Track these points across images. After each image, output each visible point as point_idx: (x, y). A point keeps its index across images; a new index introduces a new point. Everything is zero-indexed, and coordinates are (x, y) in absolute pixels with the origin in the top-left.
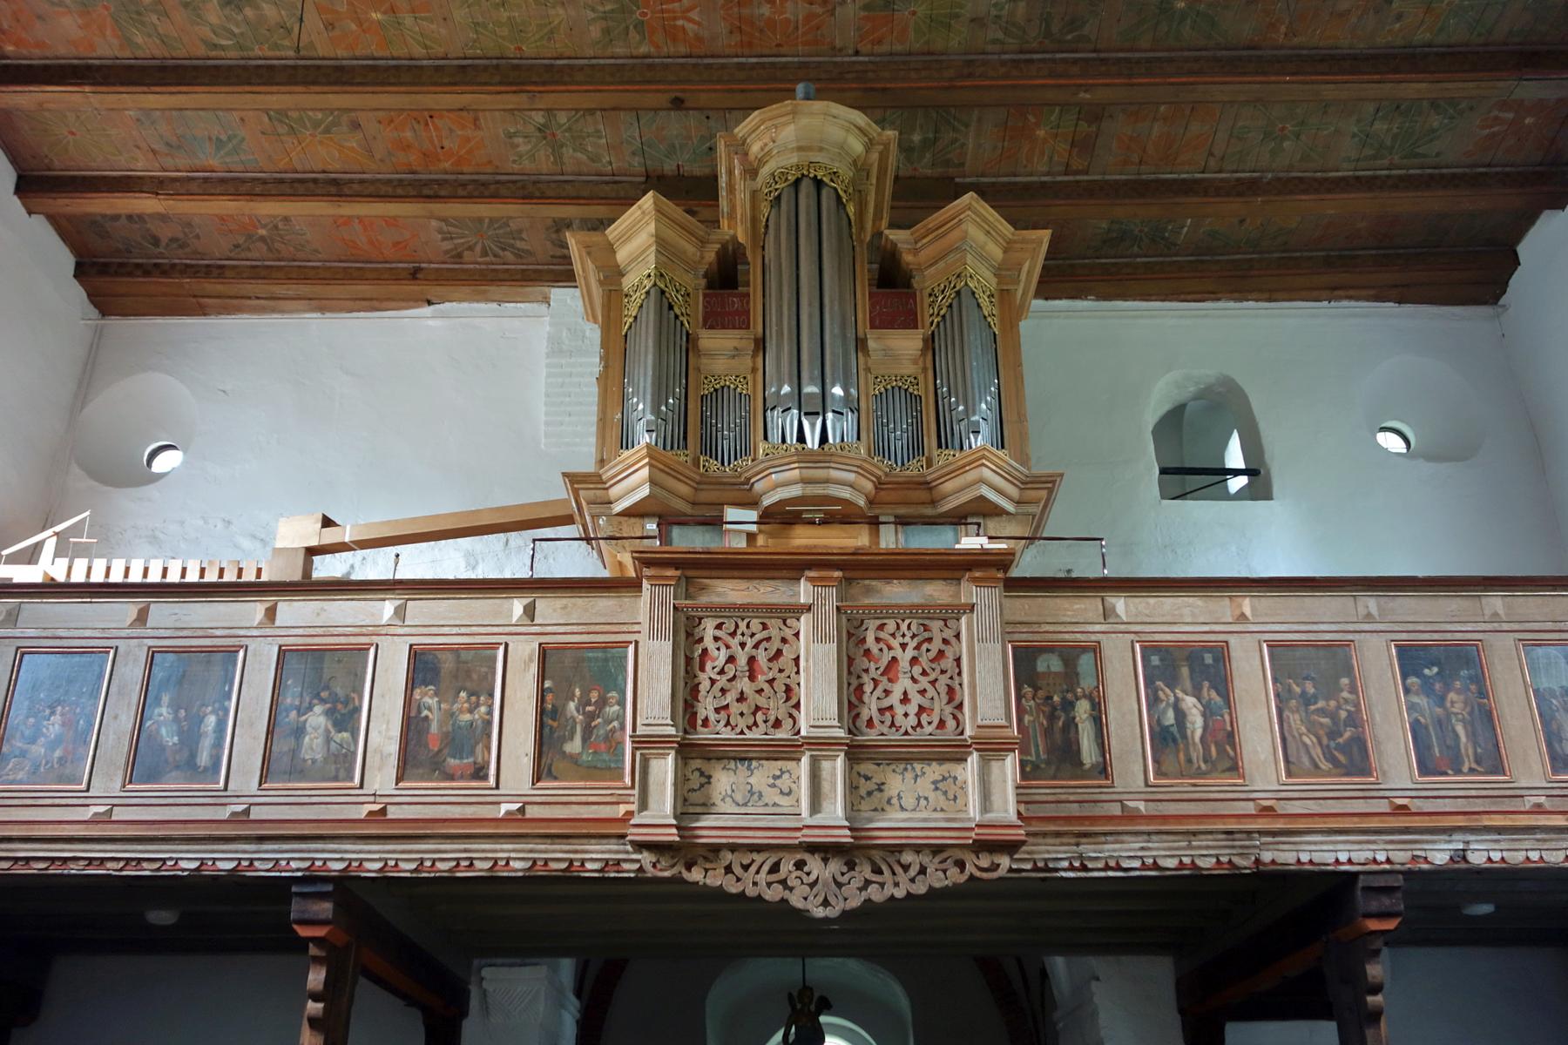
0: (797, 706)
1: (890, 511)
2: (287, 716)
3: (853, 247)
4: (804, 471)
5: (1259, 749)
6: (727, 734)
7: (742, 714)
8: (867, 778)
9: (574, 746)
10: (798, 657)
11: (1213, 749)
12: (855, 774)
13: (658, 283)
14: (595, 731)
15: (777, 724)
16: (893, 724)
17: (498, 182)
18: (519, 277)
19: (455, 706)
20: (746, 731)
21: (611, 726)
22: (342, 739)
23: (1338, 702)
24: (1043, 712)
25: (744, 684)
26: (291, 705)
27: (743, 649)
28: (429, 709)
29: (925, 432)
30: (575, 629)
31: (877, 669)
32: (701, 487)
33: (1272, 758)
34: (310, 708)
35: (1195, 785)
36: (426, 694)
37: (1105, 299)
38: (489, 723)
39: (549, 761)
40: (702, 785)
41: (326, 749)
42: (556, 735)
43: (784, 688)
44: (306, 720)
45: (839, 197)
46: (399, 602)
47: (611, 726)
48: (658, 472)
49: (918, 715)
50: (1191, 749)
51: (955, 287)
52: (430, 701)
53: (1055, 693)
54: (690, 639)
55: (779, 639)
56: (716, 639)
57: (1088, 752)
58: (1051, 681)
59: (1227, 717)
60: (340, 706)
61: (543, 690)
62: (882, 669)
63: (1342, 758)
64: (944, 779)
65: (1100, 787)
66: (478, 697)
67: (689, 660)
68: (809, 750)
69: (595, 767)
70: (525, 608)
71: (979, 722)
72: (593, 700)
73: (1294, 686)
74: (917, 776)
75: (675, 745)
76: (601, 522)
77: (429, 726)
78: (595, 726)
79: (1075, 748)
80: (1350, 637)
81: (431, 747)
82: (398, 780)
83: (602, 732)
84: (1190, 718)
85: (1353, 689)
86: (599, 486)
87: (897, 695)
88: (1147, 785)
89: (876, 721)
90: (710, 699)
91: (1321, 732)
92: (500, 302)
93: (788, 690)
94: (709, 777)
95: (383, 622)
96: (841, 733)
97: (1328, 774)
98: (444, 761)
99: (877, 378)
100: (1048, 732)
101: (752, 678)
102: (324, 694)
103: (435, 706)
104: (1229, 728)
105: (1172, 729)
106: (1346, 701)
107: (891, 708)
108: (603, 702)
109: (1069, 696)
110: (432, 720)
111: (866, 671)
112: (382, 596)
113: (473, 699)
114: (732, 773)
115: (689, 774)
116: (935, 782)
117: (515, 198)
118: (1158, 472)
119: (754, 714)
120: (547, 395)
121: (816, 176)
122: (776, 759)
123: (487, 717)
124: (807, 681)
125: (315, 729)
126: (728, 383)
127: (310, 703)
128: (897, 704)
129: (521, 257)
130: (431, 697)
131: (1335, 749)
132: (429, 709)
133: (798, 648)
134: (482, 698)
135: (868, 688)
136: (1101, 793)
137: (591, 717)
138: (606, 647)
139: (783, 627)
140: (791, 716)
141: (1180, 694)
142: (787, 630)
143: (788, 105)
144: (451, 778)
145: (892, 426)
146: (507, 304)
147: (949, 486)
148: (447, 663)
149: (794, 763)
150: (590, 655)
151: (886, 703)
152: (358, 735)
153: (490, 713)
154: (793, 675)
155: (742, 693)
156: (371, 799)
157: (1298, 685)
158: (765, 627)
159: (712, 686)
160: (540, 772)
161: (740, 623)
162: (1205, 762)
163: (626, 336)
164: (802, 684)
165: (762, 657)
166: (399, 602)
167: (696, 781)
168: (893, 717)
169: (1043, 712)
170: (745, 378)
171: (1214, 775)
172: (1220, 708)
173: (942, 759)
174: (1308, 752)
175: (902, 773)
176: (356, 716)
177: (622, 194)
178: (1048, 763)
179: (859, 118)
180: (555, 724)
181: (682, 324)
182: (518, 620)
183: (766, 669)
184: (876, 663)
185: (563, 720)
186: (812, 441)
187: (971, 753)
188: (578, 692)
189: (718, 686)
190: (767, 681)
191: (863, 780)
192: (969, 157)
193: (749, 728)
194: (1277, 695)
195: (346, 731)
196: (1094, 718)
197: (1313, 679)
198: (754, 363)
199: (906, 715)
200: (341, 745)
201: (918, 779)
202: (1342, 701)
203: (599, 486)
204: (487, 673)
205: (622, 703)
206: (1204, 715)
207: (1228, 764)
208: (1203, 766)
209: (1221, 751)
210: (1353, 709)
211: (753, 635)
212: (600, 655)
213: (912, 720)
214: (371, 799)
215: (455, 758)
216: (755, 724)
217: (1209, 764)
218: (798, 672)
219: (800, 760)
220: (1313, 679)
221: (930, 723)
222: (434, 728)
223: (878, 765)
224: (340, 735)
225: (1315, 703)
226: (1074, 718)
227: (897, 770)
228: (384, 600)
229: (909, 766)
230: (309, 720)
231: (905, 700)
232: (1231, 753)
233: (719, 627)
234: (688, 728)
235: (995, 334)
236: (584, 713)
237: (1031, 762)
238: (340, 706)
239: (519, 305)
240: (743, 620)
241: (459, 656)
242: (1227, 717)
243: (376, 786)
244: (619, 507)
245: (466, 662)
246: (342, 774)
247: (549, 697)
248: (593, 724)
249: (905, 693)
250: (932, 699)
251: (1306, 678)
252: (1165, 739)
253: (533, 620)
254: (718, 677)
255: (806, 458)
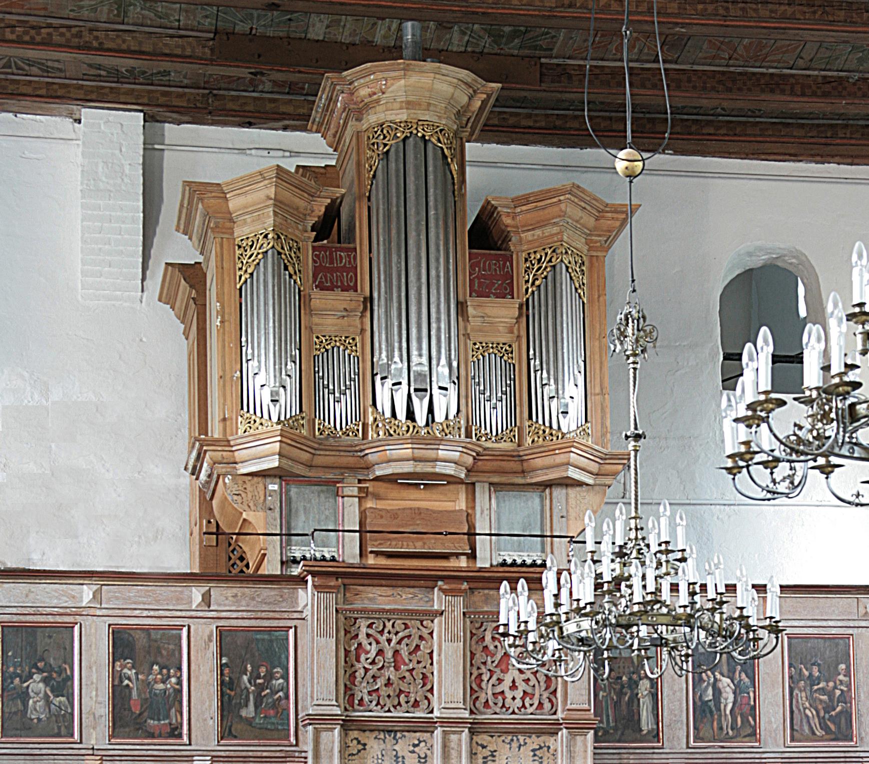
0: (431, 690)
1: (485, 479)
2: (12, 683)
3: (455, 202)
4: (416, 451)
5: (773, 720)
6: (378, 713)
7: (389, 696)
8: (484, 747)
9: (249, 712)
10: (432, 652)
11: (739, 719)
12: (474, 744)
13: (276, 246)
14: (265, 699)
15: (416, 704)
16: (503, 706)
17: (49, 26)
18: (43, 92)
19: (150, 677)
20: (392, 709)
21: (277, 696)
22: (60, 702)
23: (835, 683)
24: (614, 689)
25: (390, 673)
26: (14, 673)
27: (389, 644)
28: (129, 679)
29: (517, 402)
30: (245, 615)
31: (493, 662)
32: (318, 452)
33: (781, 727)
34: (30, 676)
35: (723, 747)
36: (125, 667)
37: (683, 153)
38: (180, 691)
39: (229, 724)
40: (359, 751)
41: (47, 710)
42: (234, 702)
43: (421, 676)
44: (28, 687)
45: (445, 157)
46: (95, 587)
47: (277, 696)
48: (288, 448)
49: (523, 699)
50: (723, 719)
51: (550, 261)
52: (129, 672)
53: (624, 674)
54: (348, 636)
55: (417, 636)
56: (368, 635)
57: (646, 722)
58: (621, 664)
59: (752, 695)
60: (55, 675)
61: (221, 665)
62: (496, 662)
63: (832, 727)
64: (541, 748)
65: (653, 748)
66: (169, 671)
67: (347, 652)
68: (441, 727)
69: (266, 729)
70: (203, 595)
71: (569, 707)
72: (262, 674)
73: (804, 670)
74: (520, 746)
75: (341, 722)
76: (227, 481)
77: (130, 693)
78: (265, 696)
79: (636, 717)
80: (850, 631)
81: (133, 709)
82: (111, 737)
83: (270, 700)
84: (724, 695)
85: (848, 674)
86: (227, 449)
87: (507, 682)
88: (688, 747)
89: (491, 703)
90: (364, 684)
91: (820, 707)
92: (15, 113)
93: (424, 677)
94: (365, 745)
95: (84, 605)
96: (466, 714)
97: (821, 739)
98: (146, 721)
99: (475, 344)
100: (617, 705)
101: (397, 668)
102: (41, 665)
103: (133, 677)
104: (752, 703)
105: (710, 703)
106: (841, 682)
107: (503, 692)
108: (270, 676)
109: (635, 677)
110: (132, 688)
111: (485, 663)
112: (81, 582)
113: (165, 671)
114: (381, 742)
115: (348, 741)
116: (533, 750)
117: (69, 47)
118: (722, 359)
119: (398, 696)
120: (84, 241)
121: (424, 136)
122: (415, 732)
123: (177, 687)
124: (440, 671)
125: (37, 694)
126: (338, 344)
127: (30, 672)
128: (507, 690)
129: (48, 72)
130: (130, 670)
131: (829, 720)
132: (129, 679)
133: (432, 646)
134: (172, 671)
135: (485, 678)
136: (653, 753)
137: (261, 688)
138: (271, 630)
139: (421, 627)
140: (426, 698)
141: (718, 676)
142: (424, 629)
143: (400, 64)
144: (152, 736)
145: (488, 394)
146: (24, 116)
147: (539, 462)
148: (141, 640)
149: (429, 734)
150: (258, 637)
151: (498, 689)
152: (73, 699)
153: (180, 682)
154: (428, 666)
155: (389, 679)
156: (91, 752)
157: (807, 670)
158: (406, 627)
159: (365, 674)
160: (226, 733)
161: (387, 624)
162: (732, 729)
163: (241, 289)
164: (435, 673)
165: (404, 653)
166: (95, 587)
167: (354, 747)
168: (504, 700)
169: (614, 689)
170: (354, 339)
171: (739, 739)
172: (748, 687)
173: (540, 733)
174: (808, 722)
175: (510, 743)
176: (69, 683)
177: (188, 52)
178: (616, 729)
179: (464, 74)
180: (233, 693)
181: (295, 282)
182: (197, 606)
183: (407, 661)
184: (492, 657)
185: (238, 689)
186: (421, 416)
187: (561, 729)
188: (249, 667)
189: (370, 673)
190: (408, 670)
191: (480, 748)
192: (558, 45)
193: (395, 707)
194: (791, 677)
195: (63, 696)
196: (653, 695)
197: (819, 665)
198: (362, 323)
199: (514, 698)
200: (59, 707)
201: (522, 748)
202: (838, 682)
203: (227, 449)
204: (174, 650)
205: (286, 677)
206: (734, 693)
207: (749, 731)
208: (731, 733)
209: (745, 721)
210: (845, 689)
211: (397, 633)
212: (266, 637)
213: (518, 702)
214: (91, 752)
215: (154, 719)
216: (399, 704)
217: (735, 731)
218: (432, 664)
219: (433, 732)
220: (819, 665)
221: (531, 705)
222: (134, 694)
223: (492, 736)
224: (58, 699)
225: (818, 684)
226: (637, 694)
227: (507, 741)
228: (82, 584)
229: (515, 738)
230: (31, 686)
231: (514, 687)
232: (752, 722)
233: (370, 626)
234: (347, 706)
235: (583, 303)
236: (255, 685)
237: (603, 728)
238: (55, 675)
239: (38, 117)
240: (389, 620)
241: (149, 635)
242: (752, 695)
243: (93, 742)
244: (244, 469)
245: (156, 641)
246: (63, 731)
247: (226, 671)
248: (263, 694)
249: (514, 681)
250: (534, 686)
251: (814, 664)
252: (704, 711)
253: (209, 606)
254: (370, 667)
255: (416, 439)
